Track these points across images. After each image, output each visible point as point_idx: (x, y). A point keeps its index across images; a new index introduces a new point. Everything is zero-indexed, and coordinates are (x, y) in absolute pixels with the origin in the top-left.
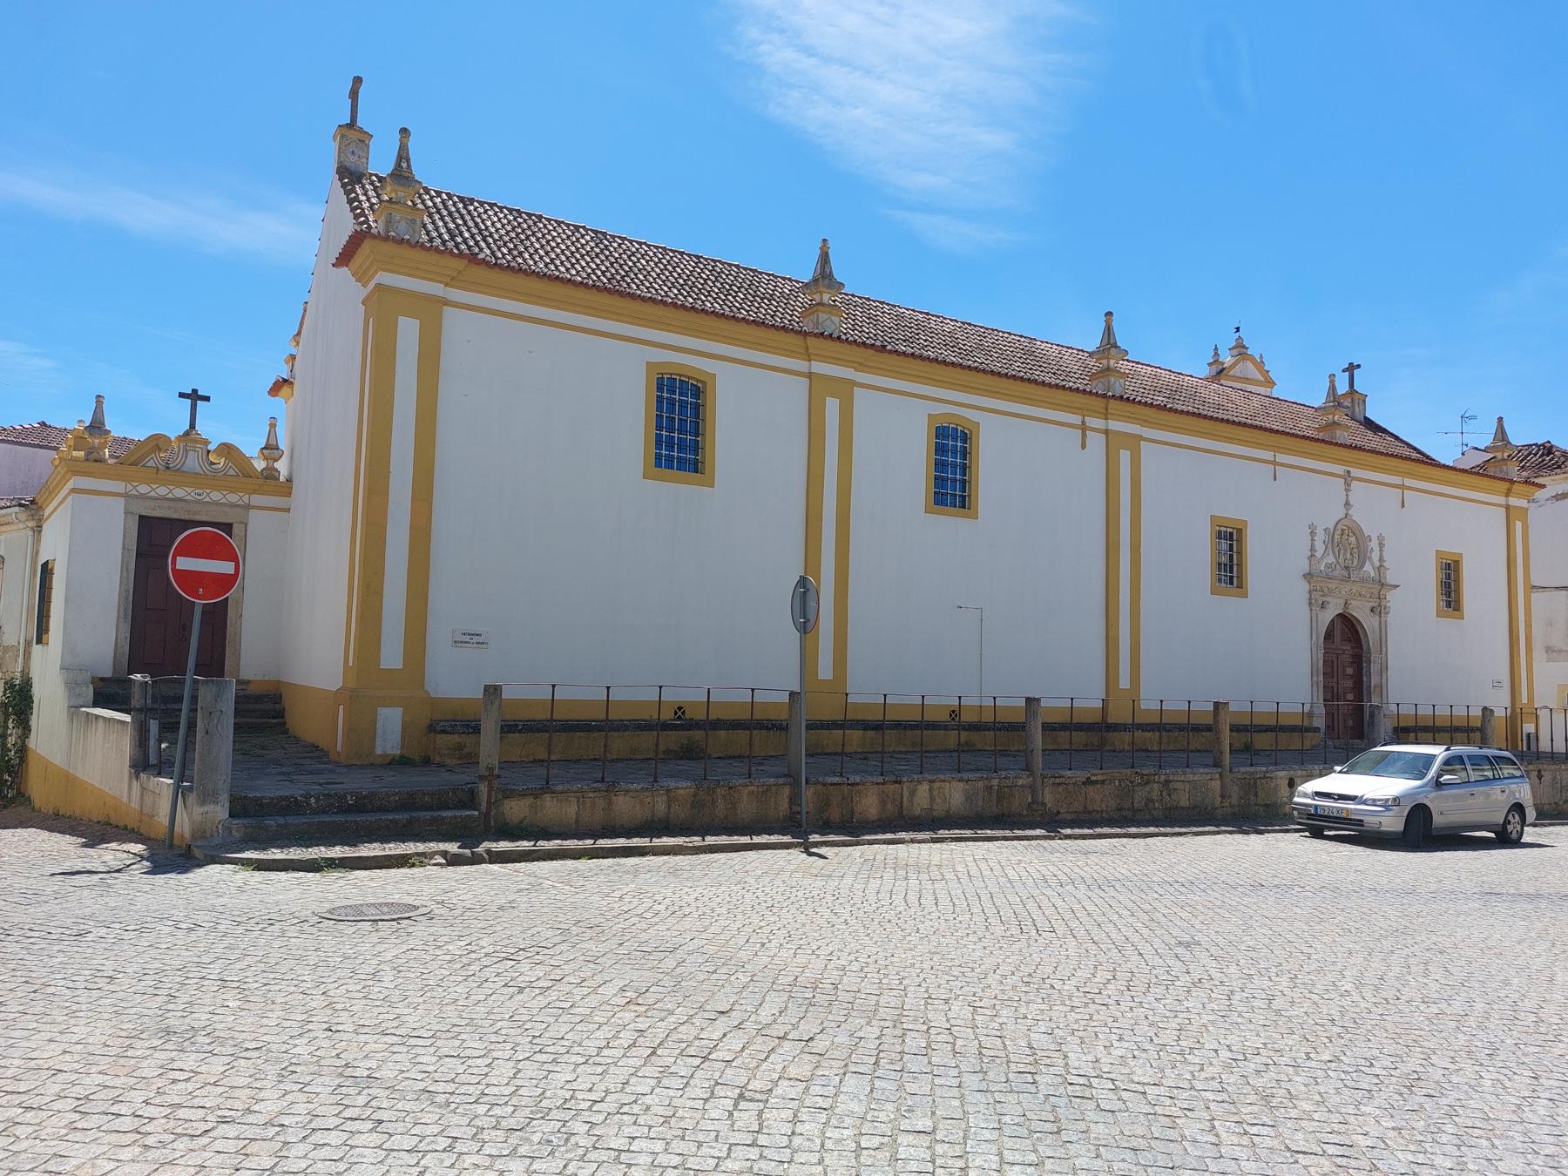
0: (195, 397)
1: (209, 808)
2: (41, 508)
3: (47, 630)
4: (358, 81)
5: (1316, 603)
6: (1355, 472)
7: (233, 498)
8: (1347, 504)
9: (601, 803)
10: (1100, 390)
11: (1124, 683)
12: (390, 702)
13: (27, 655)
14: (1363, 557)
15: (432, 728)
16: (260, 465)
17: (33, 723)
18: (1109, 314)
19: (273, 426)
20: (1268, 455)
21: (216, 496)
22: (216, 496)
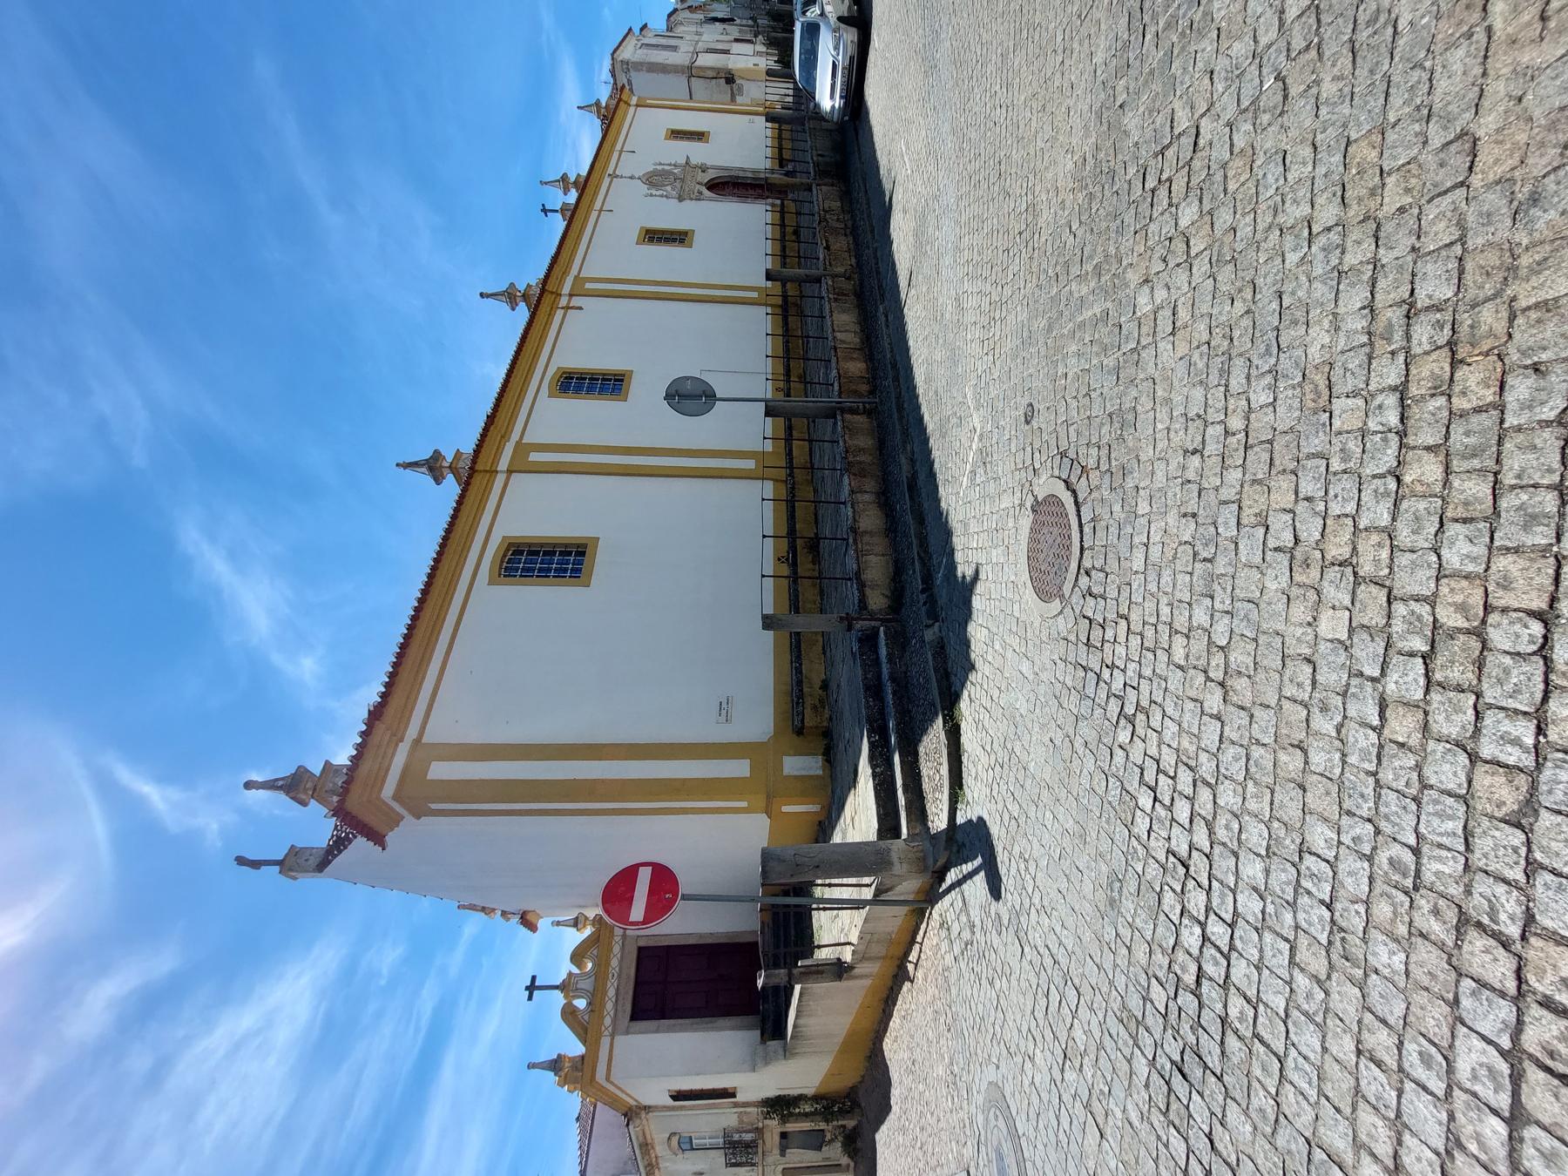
0: (532, 988)
1: (894, 857)
2: (630, 1108)
3: (725, 1090)
4: (241, 861)
5: (699, 197)
6: (610, 171)
7: (616, 949)
8: (632, 178)
9: (866, 538)
10: (540, 303)
11: (755, 295)
12: (779, 766)
13: (746, 1105)
14: (670, 173)
15: (799, 732)
16: (588, 931)
17: (795, 1092)
18: (482, 295)
19: (558, 923)
20: (594, 215)
21: (615, 962)
22: (615, 962)
